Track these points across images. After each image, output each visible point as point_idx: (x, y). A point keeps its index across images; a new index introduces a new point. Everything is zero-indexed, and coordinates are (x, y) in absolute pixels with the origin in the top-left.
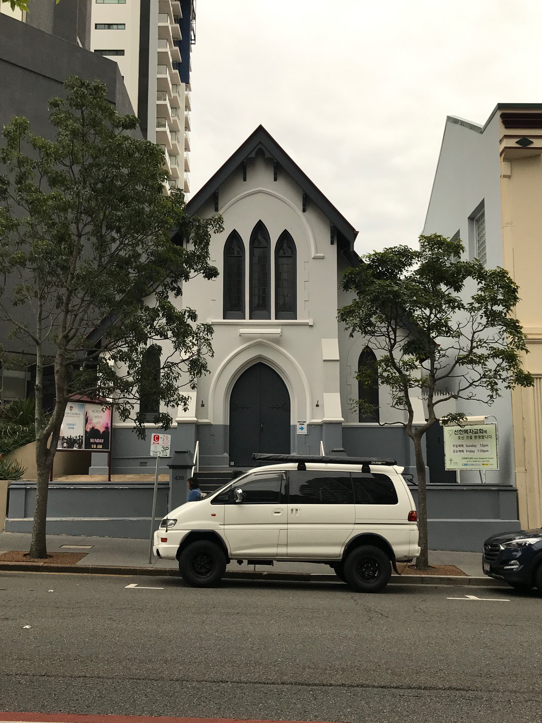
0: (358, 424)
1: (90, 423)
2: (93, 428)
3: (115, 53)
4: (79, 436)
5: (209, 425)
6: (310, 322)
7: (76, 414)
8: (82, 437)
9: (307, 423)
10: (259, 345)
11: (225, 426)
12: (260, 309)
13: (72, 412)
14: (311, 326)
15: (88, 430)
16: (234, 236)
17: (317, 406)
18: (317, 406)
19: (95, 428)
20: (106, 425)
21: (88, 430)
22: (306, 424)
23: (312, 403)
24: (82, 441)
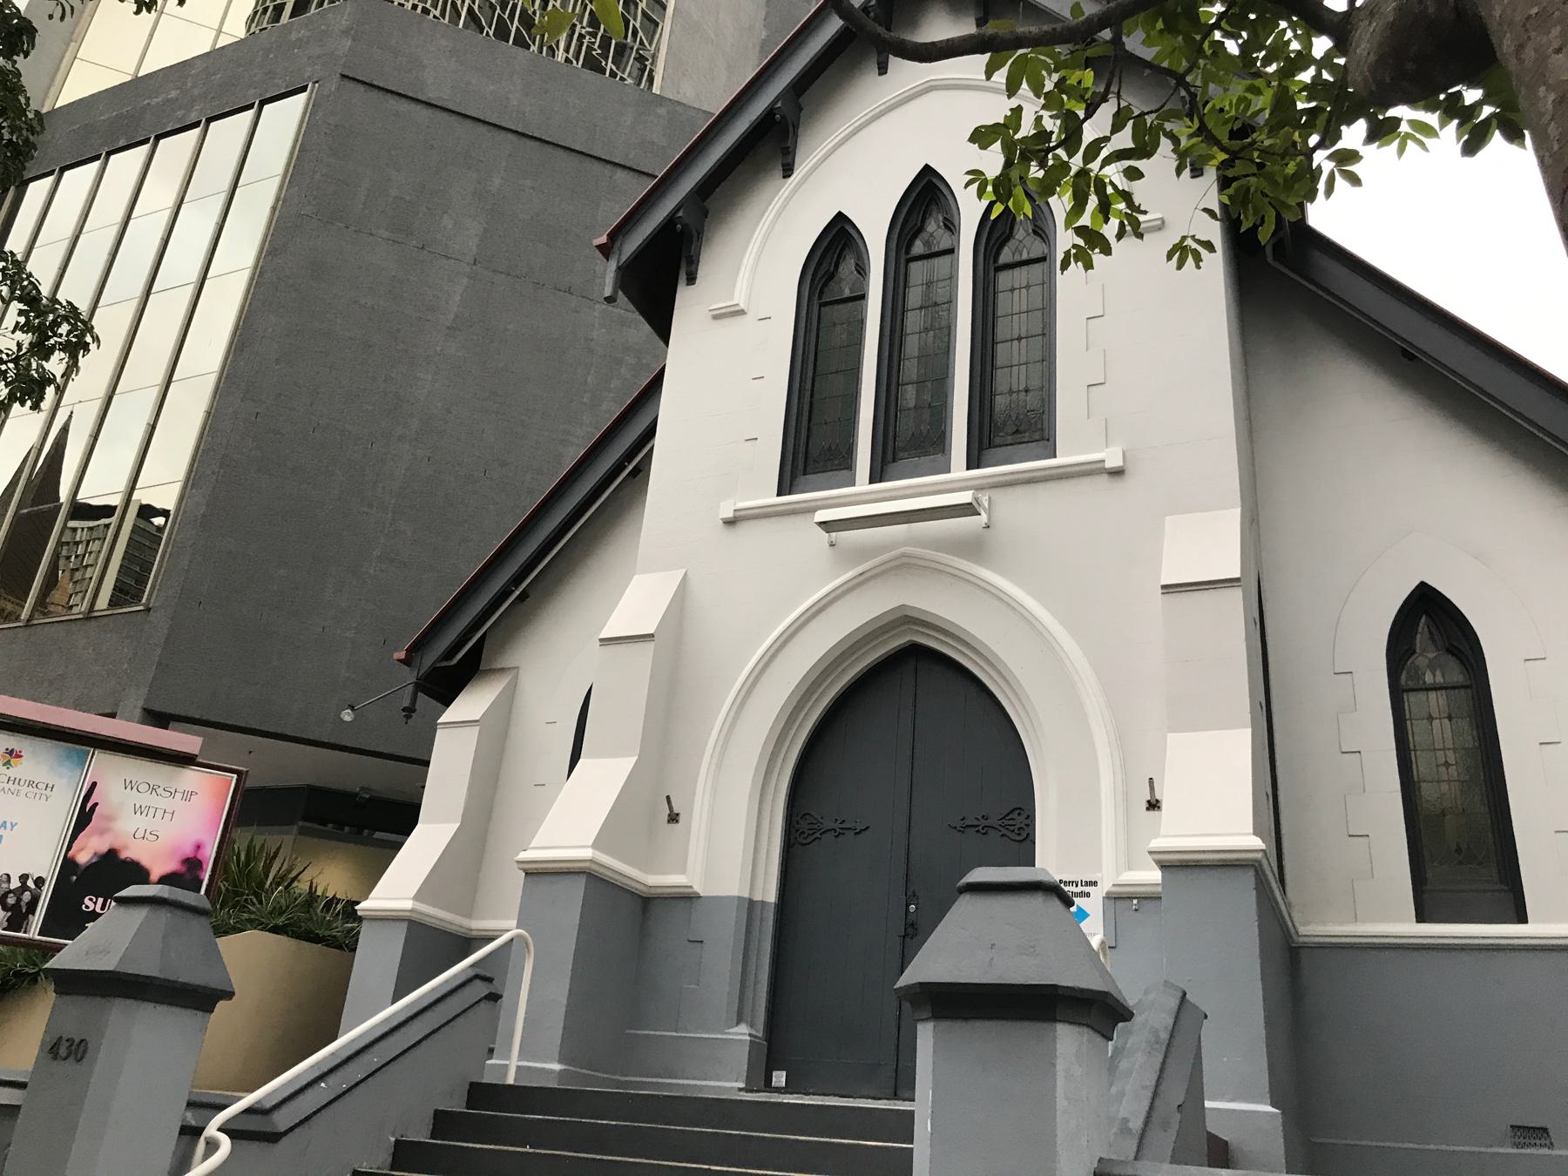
0: (1408, 928)
1: (102, 832)
2: (112, 853)
3: (1445, 784)
4: (24, 878)
5: (686, 899)
6: (1114, 462)
7: (30, 784)
8: (40, 882)
9: (1105, 887)
10: (902, 566)
11: (752, 906)
12: (908, 442)
13: (13, 772)
14: (1117, 473)
15: (83, 858)
16: (839, 238)
17: (1153, 805)
18: (1153, 805)
19: (124, 855)
20: (188, 851)
21: (83, 858)
22: (1097, 894)
23: (1126, 794)
24: (35, 900)
